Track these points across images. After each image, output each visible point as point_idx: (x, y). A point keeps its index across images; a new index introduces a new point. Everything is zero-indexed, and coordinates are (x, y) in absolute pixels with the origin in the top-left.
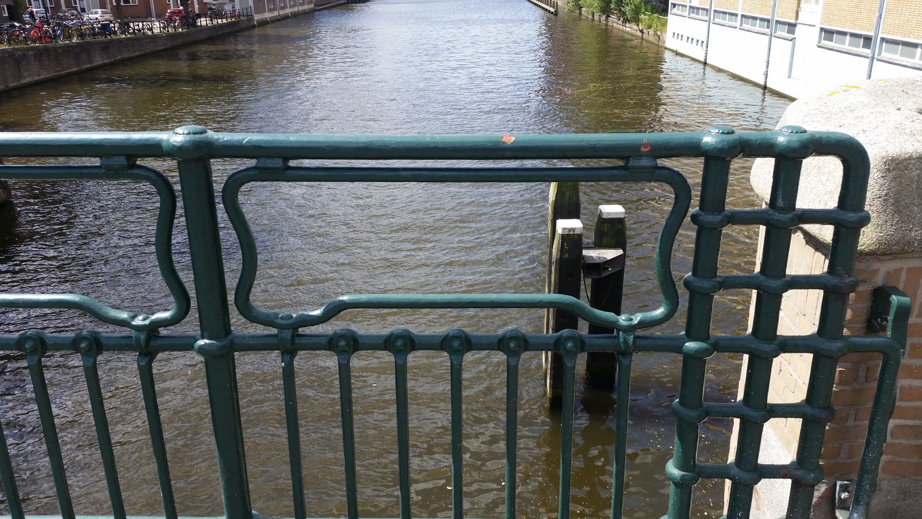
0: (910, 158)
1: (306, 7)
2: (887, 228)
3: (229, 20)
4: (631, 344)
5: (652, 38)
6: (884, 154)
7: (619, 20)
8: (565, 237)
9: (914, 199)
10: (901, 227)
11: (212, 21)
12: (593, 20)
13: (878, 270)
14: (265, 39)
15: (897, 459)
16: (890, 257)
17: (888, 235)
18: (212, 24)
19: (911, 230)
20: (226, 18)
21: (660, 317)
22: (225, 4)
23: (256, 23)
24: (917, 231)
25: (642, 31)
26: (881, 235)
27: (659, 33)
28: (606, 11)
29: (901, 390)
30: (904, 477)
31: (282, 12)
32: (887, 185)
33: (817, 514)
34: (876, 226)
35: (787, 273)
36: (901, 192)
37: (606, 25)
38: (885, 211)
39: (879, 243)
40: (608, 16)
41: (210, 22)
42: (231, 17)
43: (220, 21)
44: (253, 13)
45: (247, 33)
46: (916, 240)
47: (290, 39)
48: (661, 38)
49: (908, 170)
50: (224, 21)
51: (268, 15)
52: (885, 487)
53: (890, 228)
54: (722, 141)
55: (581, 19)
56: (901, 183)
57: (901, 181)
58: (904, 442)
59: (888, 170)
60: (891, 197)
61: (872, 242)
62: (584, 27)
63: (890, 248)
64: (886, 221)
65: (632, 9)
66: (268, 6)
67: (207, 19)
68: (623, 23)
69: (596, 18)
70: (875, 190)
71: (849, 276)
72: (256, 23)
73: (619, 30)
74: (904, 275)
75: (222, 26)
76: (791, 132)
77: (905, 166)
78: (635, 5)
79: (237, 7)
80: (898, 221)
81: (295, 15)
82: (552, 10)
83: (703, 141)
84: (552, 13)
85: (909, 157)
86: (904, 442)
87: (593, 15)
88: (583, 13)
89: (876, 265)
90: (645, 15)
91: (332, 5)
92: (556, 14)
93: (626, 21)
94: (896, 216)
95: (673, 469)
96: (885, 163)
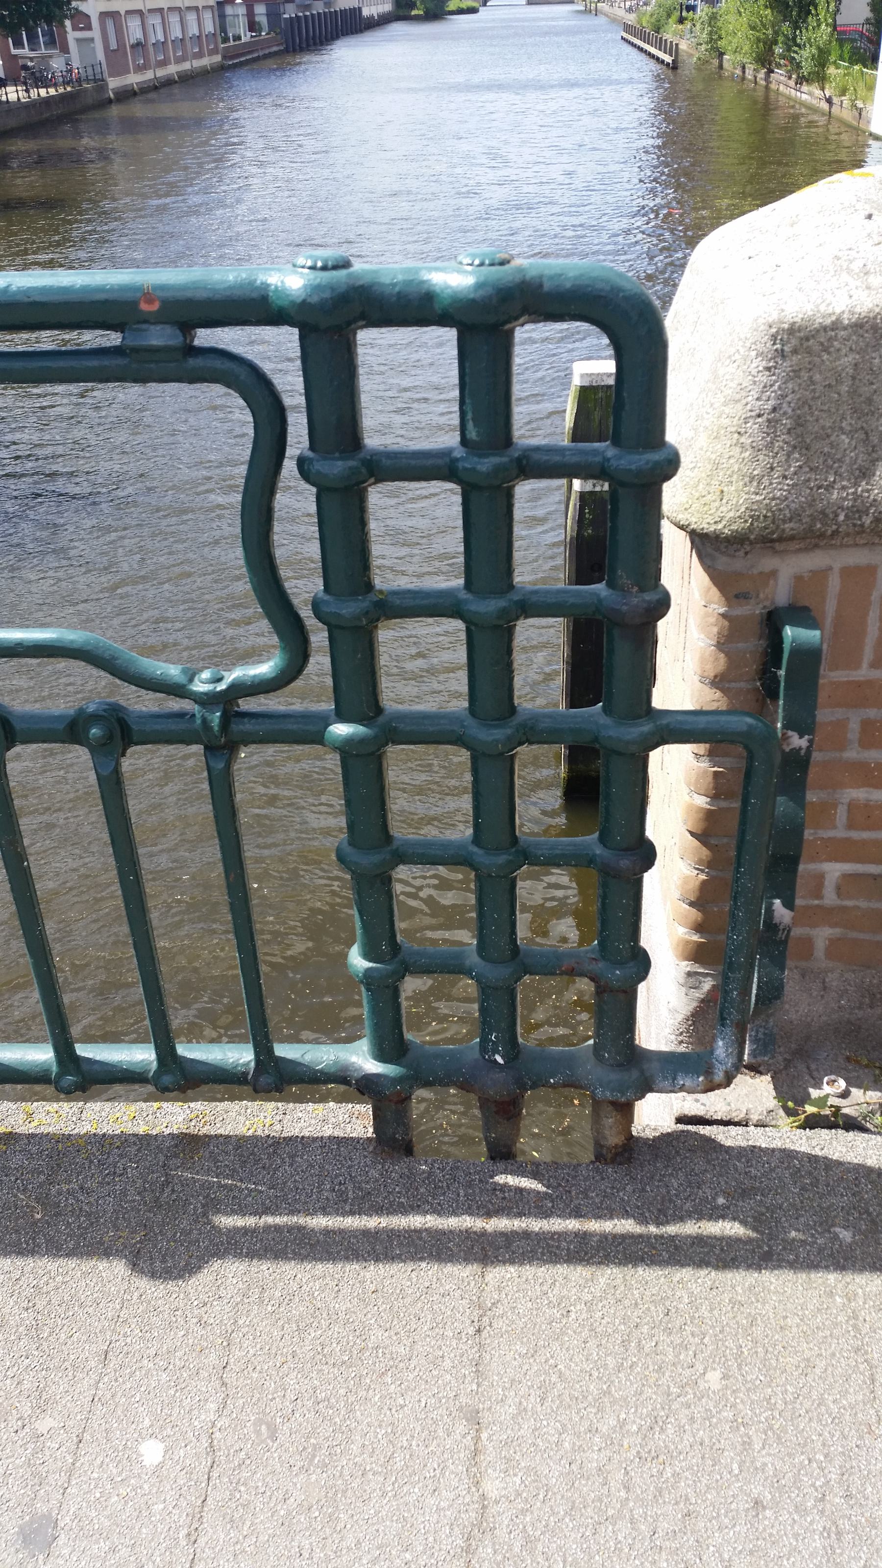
0: (836, 325)
1: (206, 61)
2: (771, 484)
3: (61, 90)
4: (216, 728)
5: (847, 115)
6: (774, 316)
7: (790, 78)
8: (587, 496)
9: (843, 418)
10: (809, 480)
11: (27, 91)
12: (743, 78)
13: (774, 574)
14: (131, 126)
15: (854, 935)
16: (794, 545)
17: (773, 499)
18: (29, 97)
19: (830, 487)
20: (55, 85)
21: (273, 675)
22: (51, 57)
23: (112, 96)
24: (844, 488)
25: (829, 101)
26: (758, 498)
27: (860, 104)
28: (765, 60)
29: (849, 811)
30: (869, 967)
31: (161, 73)
32: (776, 387)
33: (701, 1028)
34: (747, 479)
35: (517, 579)
36: (811, 403)
37: (767, 88)
38: (770, 446)
39: (751, 517)
40: (771, 71)
41: (26, 95)
42: (66, 83)
43: (43, 92)
44: (106, 74)
45: (97, 115)
46: (842, 508)
47: (178, 124)
48: (863, 113)
49: (829, 353)
50: (52, 91)
51: (133, 79)
52: (834, 984)
53: (780, 483)
54: (318, 288)
55: (720, 77)
56: (813, 383)
57: (811, 378)
58: (863, 904)
59: (781, 354)
60: (785, 413)
61: (738, 514)
62: (727, 92)
63: (778, 527)
64: (772, 469)
65: (813, 56)
66: (134, 61)
67: (19, 88)
68: (796, 84)
69: (749, 75)
70: (750, 398)
71: (642, 590)
72: (112, 96)
73: (789, 98)
74: (834, 583)
75: (47, 102)
76: (482, 264)
77: (822, 344)
78: (819, 48)
79: (76, 64)
80: (800, 467)
81: (186, 79)
82: (668, 59)
83: (259, 282)
84: (668, 64)
85: (833, 323)
86: (863, 904)
87: (744, 68)
88: (726, 65)
89: (768, 563)
90: (837, 68)
91: (255, 55)
92: (674, 67)
93: (801, 80)
94: (797, 455)
95: (358, 961)
96: (774, 338)
